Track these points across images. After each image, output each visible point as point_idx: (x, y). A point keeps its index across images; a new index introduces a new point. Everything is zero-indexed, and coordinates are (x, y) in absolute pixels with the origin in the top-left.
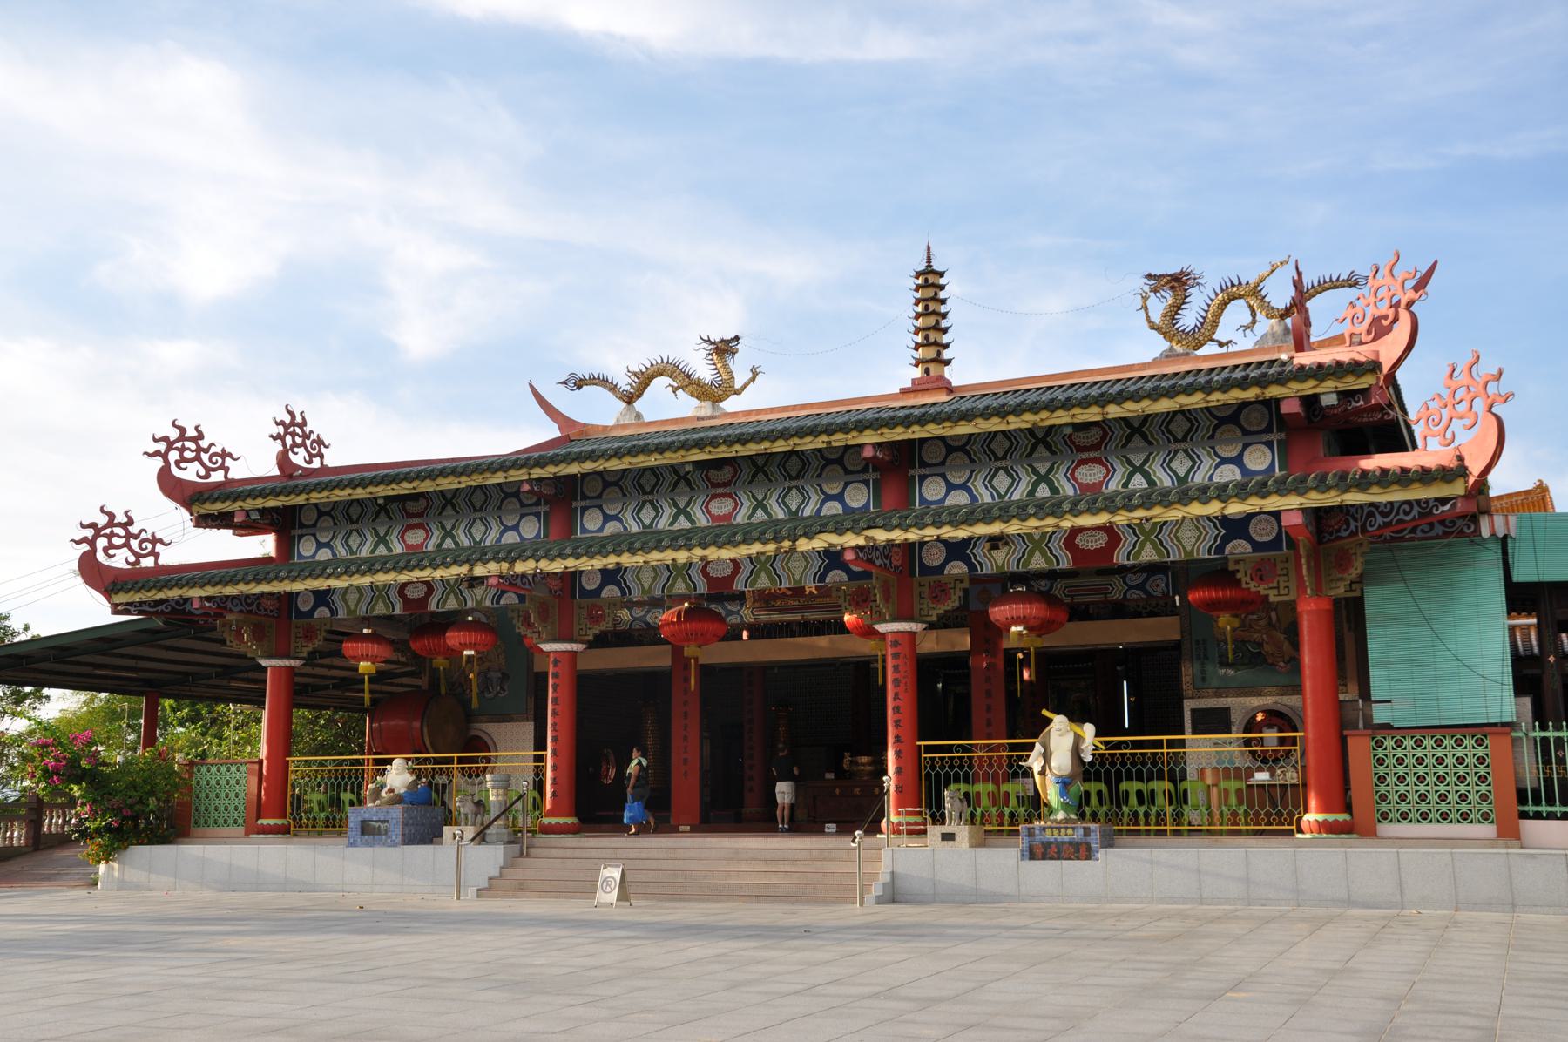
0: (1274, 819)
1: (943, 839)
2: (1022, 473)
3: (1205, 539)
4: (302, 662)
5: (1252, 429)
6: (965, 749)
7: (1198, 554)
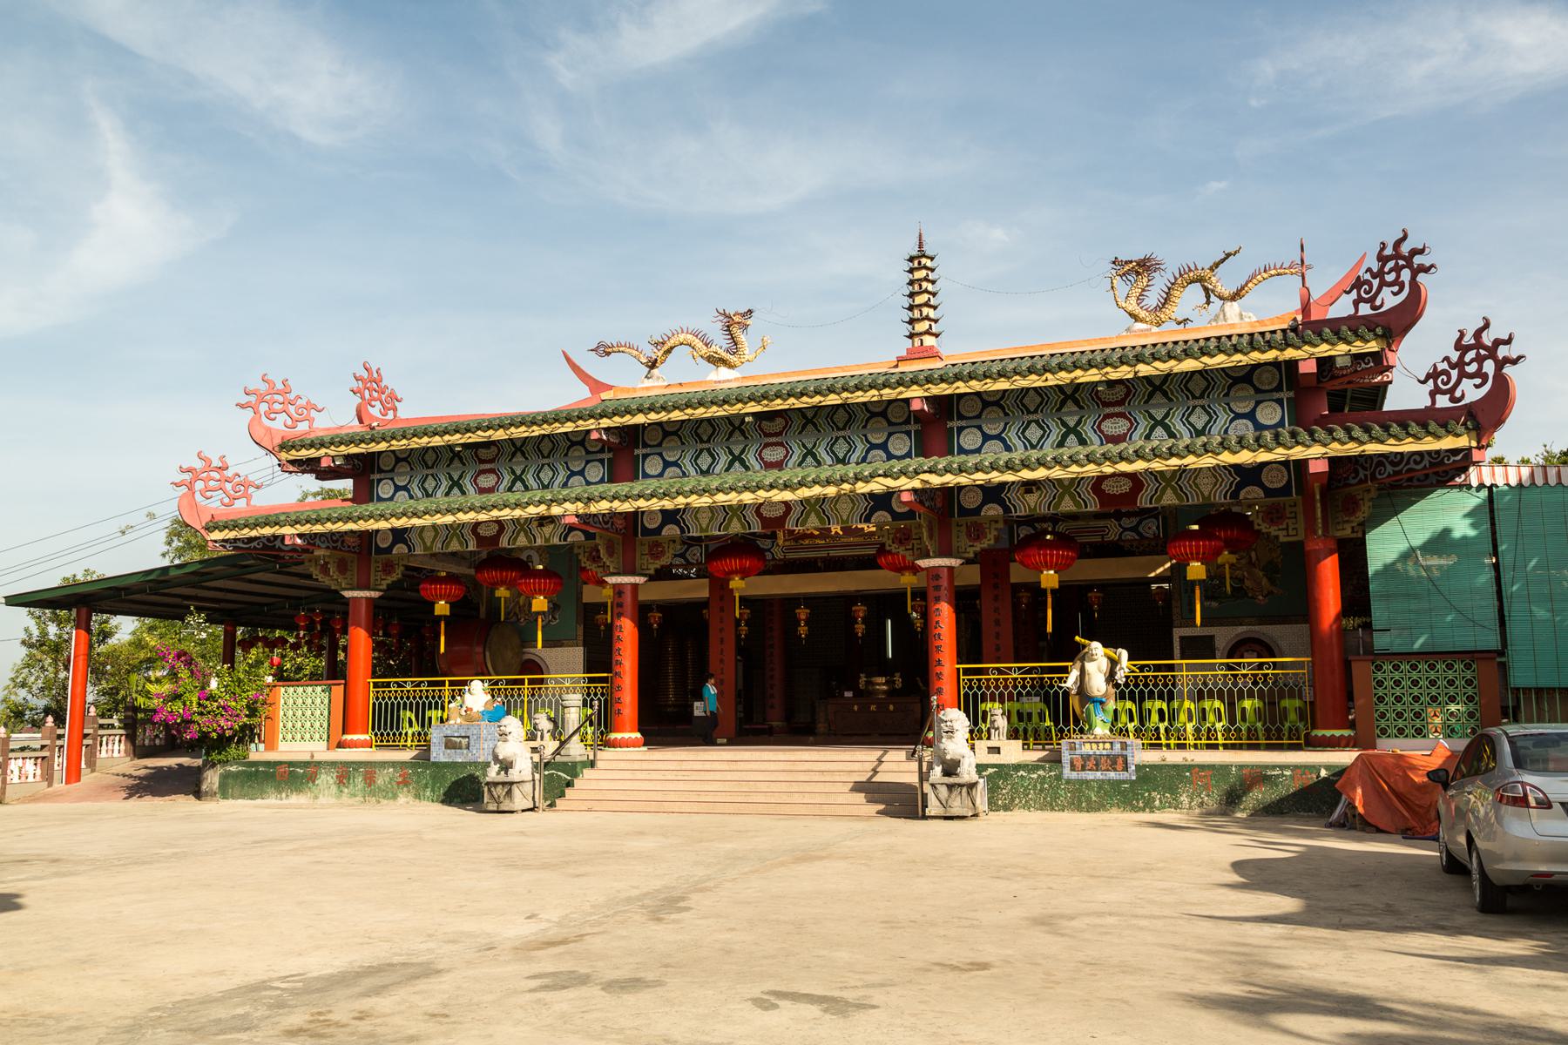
0: (1233, 735)
1: (999, 748)
2: (560, 468)
3: (1221, 485)
4: (381, 593)
5: (1263, 388)
6: (1000, 671)
7: (1215, 498)
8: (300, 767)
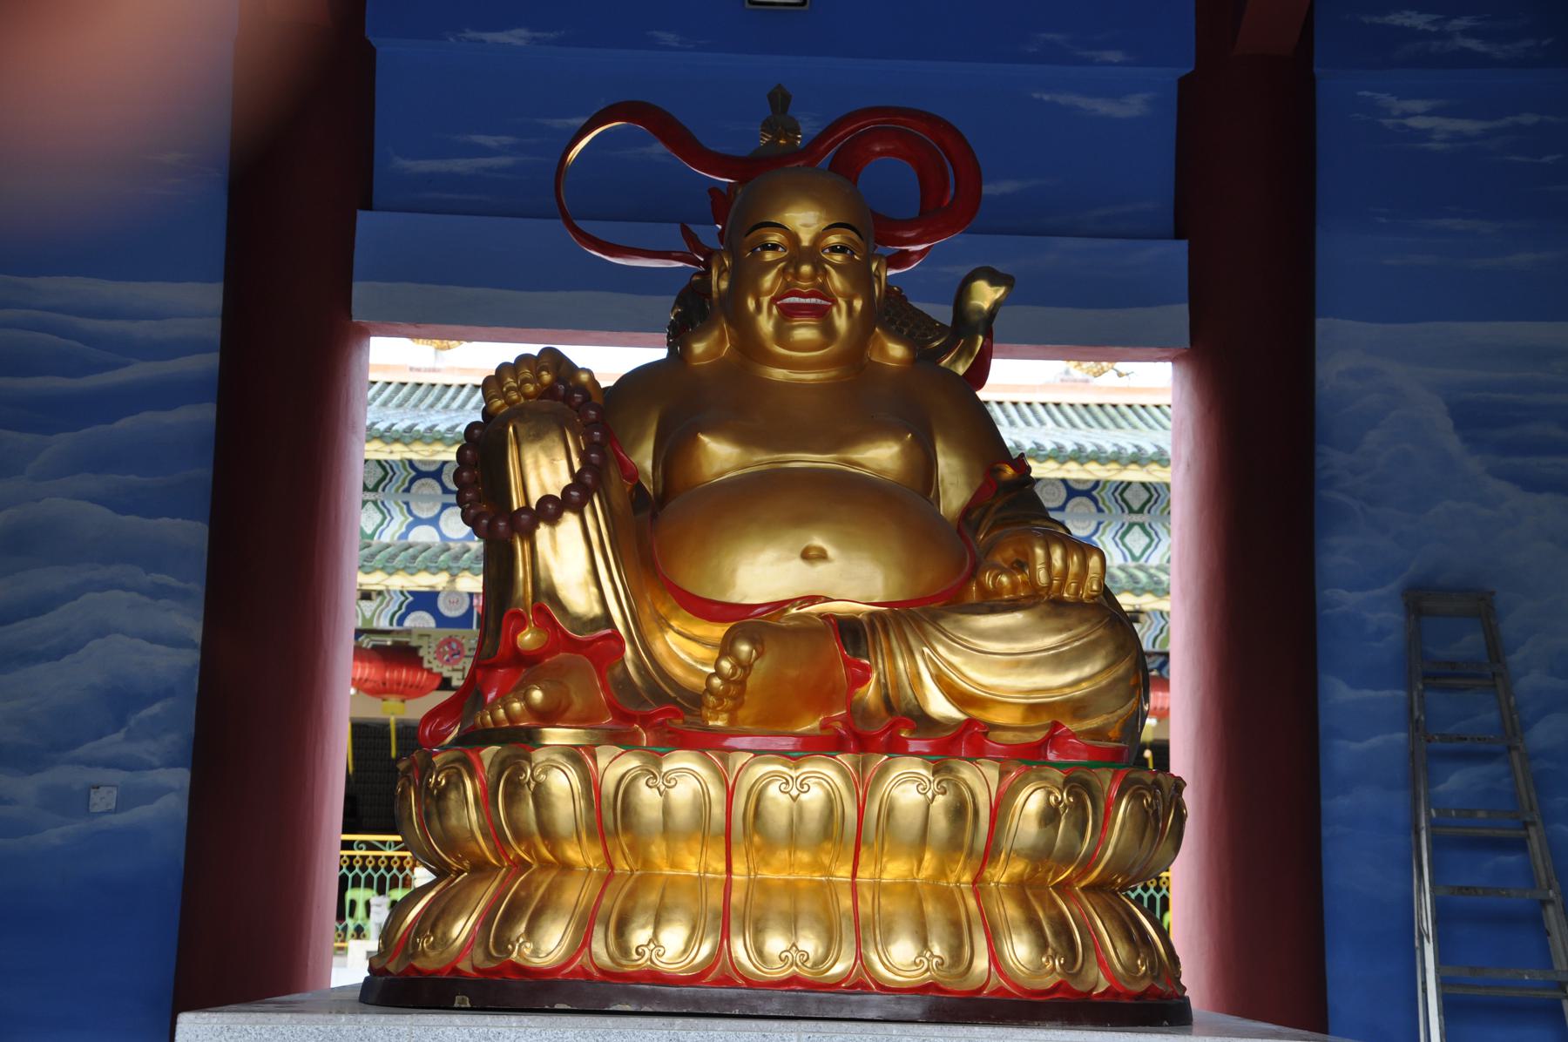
2: (396, 512)
6: (370, 846)
8: (546, 1009)
